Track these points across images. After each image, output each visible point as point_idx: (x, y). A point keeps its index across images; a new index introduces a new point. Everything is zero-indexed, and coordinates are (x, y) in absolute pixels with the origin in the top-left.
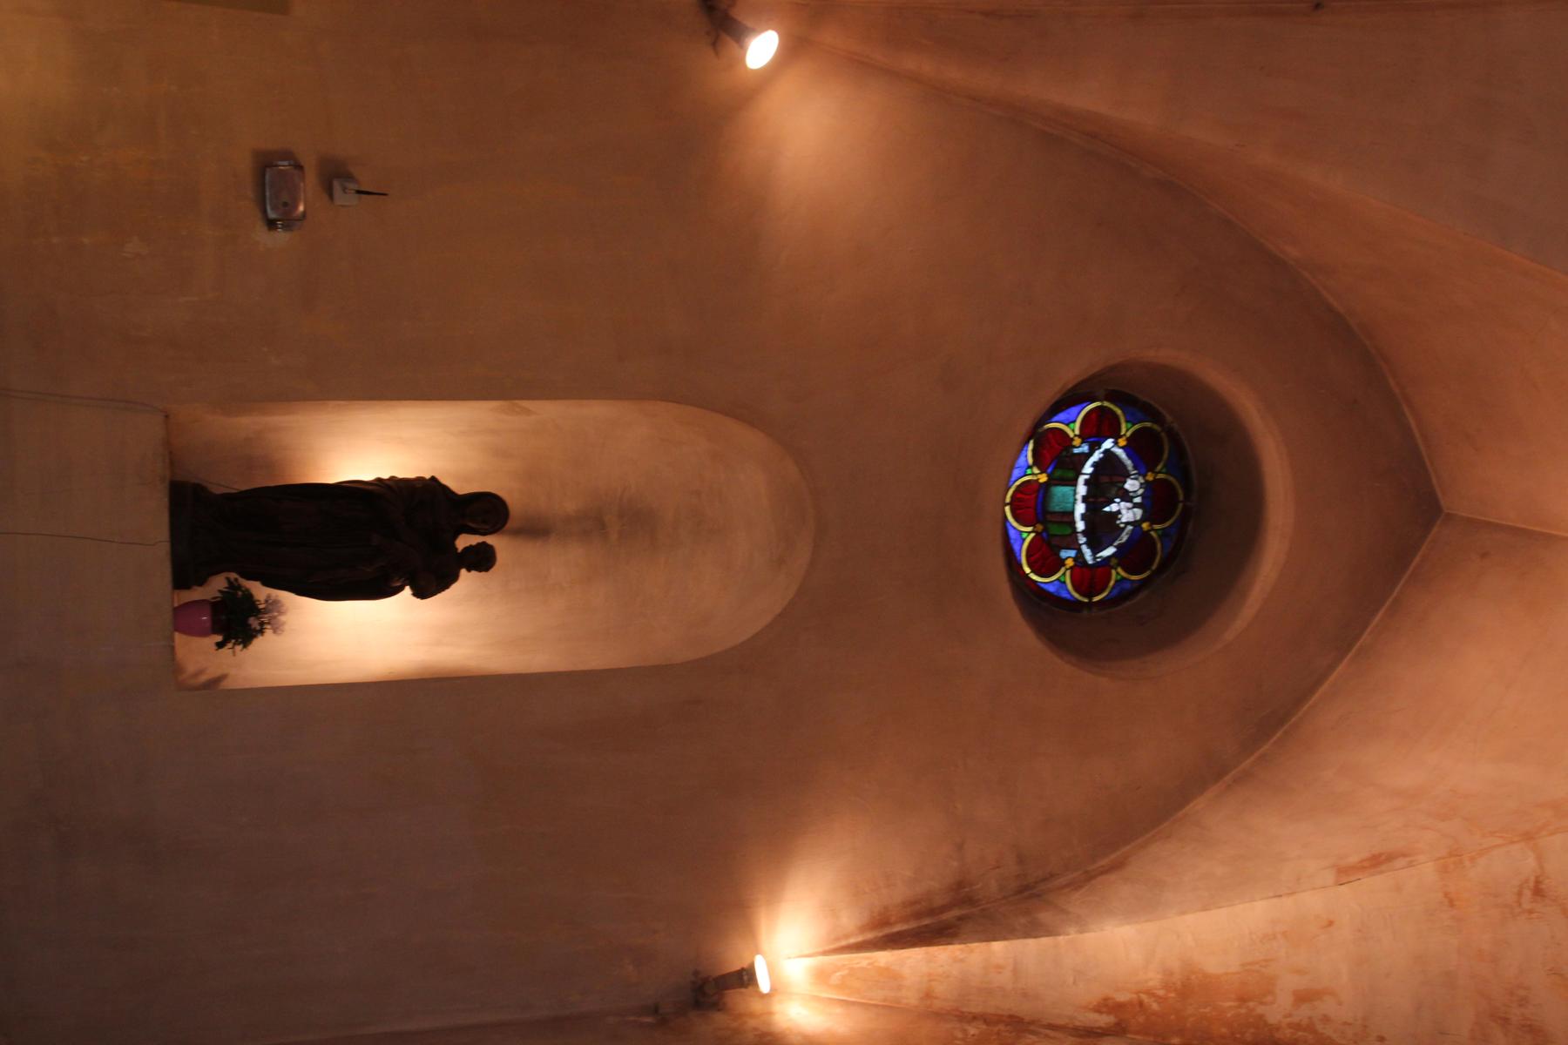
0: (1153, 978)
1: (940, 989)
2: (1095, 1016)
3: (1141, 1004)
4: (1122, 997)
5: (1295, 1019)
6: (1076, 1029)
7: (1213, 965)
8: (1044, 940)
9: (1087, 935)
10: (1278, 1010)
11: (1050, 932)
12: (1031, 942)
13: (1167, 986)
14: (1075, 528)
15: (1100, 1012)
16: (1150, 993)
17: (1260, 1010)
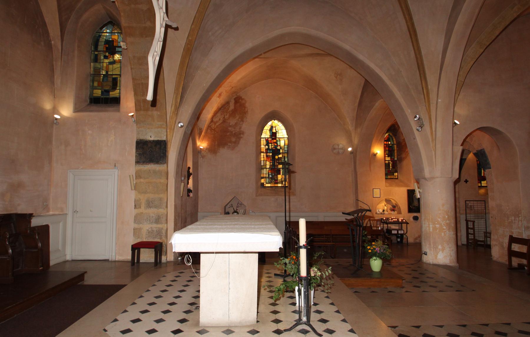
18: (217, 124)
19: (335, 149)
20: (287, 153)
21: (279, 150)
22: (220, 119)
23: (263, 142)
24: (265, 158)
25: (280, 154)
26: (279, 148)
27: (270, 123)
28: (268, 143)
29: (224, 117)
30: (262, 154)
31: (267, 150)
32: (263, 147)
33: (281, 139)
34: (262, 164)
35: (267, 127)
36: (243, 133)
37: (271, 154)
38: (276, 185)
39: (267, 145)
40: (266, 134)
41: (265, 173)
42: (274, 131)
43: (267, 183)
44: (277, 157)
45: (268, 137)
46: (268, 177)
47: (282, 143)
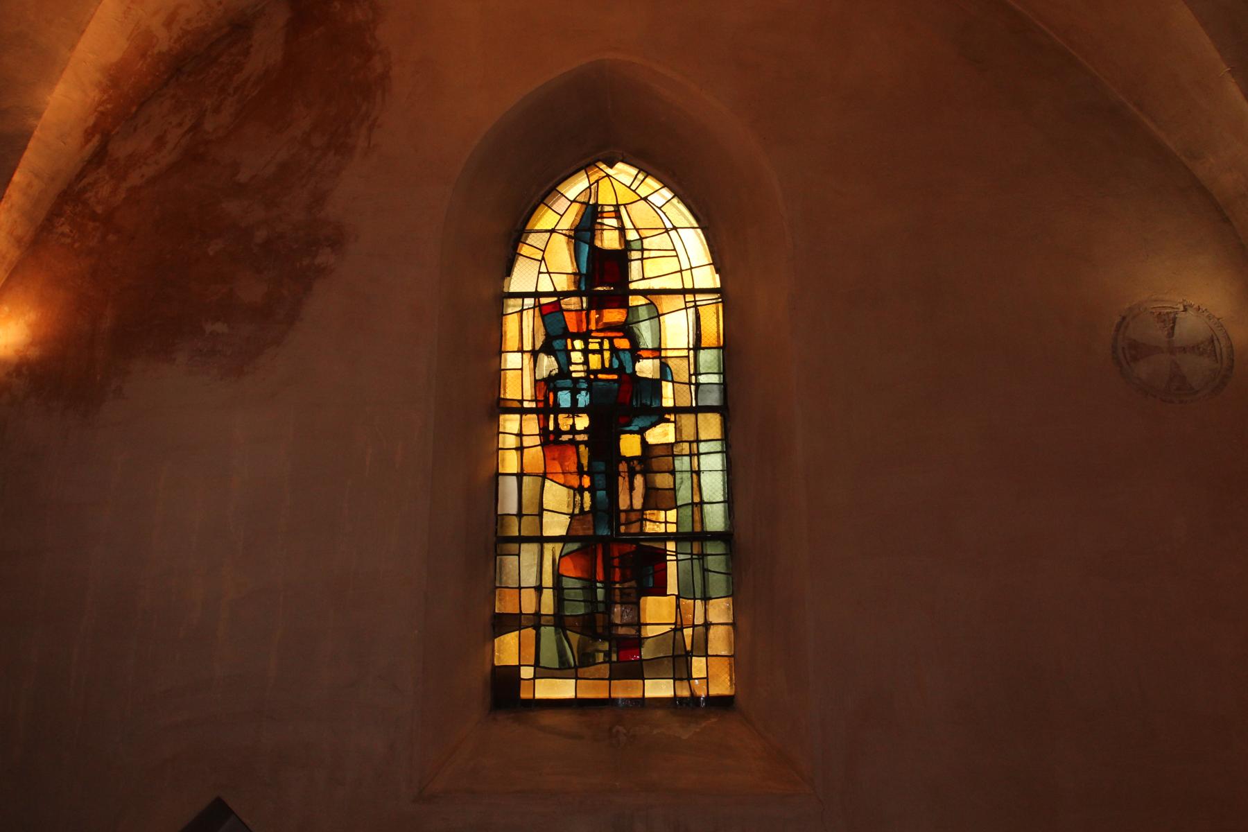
0: (95, 95)
1: (19, 231)
2: (91, 144)
3: (102, 113)
4: (91, 121)
5: (175, 36)
6: (89, 162)
7: (114, 56)
8: (31, 144)
9: (45, 114)
10: (164, 42)
11: (27, 136)
12: (27, 154)
13: (104, 91)
14: (496, 377)
15: (90, 140)
16: (101, 103)
17: (156, 51)
18: (135, 179)
19: (1138, 351)
20: (723, 410)
21: (654, 387)
22: (160, 141)
23: (520, 327)
24: (535, 456)
25: (660, 415)
26: (647, 368)
27: (576, 187)
28: (554, 340)
29: (196, 128)
30: (510, 423)
31: (547, 386)
32: (519, 374)
33: (666, 303)
34: (509, 505)
35: (558, 216)
36: (337, 241)
37: (582, 422)
38: (624, 690)
39: (548, 349)
40: (545, 265)
41: (529, 579)
42: (609, 240)
43: (542, 672)
44: (630, 445)
45: (563, 284)
46: (560, 621)
47: (676, 330)
